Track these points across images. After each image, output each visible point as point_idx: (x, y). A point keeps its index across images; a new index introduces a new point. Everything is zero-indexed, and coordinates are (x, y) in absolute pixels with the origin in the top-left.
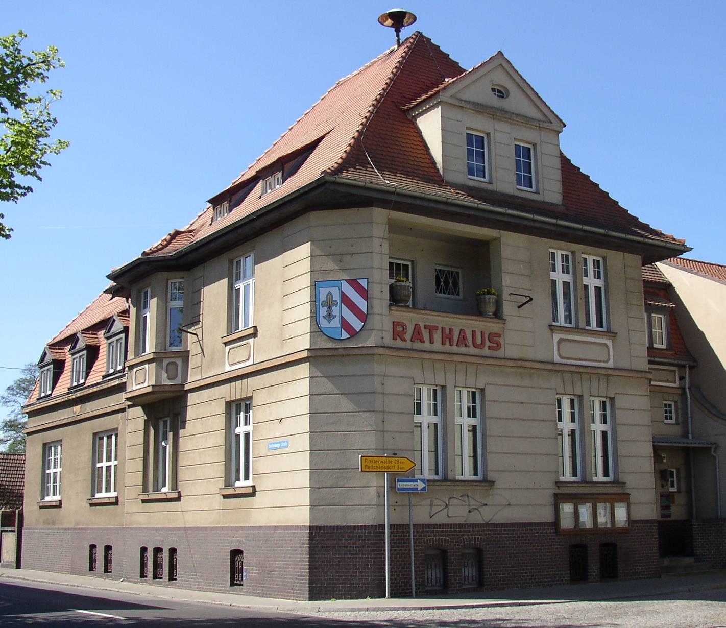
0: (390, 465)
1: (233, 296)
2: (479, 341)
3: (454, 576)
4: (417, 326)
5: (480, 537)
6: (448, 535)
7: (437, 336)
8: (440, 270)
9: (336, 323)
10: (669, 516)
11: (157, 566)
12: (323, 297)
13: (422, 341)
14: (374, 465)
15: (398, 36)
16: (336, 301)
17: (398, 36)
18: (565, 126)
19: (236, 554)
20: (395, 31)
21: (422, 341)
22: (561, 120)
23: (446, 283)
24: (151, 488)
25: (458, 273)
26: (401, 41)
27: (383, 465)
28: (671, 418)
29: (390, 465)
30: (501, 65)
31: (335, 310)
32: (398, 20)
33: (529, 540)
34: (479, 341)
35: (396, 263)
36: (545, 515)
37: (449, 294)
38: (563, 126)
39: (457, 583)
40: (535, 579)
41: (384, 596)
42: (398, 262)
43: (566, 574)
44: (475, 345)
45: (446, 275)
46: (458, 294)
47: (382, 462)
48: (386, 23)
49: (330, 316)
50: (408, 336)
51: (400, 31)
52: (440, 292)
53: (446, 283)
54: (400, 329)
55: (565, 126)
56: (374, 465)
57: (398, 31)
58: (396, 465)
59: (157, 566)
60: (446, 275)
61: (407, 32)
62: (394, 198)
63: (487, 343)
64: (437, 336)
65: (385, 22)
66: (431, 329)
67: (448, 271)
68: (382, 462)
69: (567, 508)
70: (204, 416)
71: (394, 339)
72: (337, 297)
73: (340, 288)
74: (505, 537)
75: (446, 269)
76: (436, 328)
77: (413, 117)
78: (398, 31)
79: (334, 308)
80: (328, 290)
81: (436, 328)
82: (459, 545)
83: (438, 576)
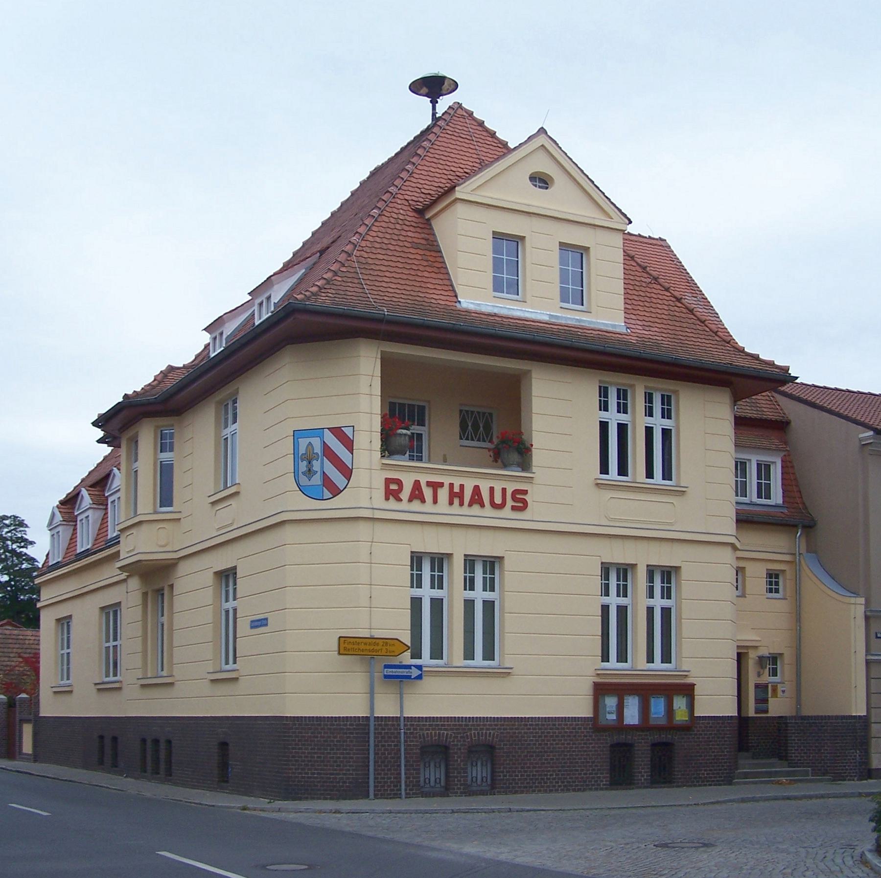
0: (376, 647)
1: (224, 449)
2: (498, 500)
3: (457, 777)
4: (417, 484)
5: (492, 732)
6: (452, 729)
7: (443, 494)
8: (467, 411)
9: (317, 480)
10: (767, 711)
11: (156, 761)
12: (302, 450)
13: (423, 501)
14: (356, 647)
15: (434, 108)
16: (317, 454)
17: (434, 108)
18: (630, 222)
19: (224, 745)
20: (431, 102)
21: (423, 501)
22: (625, 216)
23: (476, 427)
24: (111, 674)
25: (491, 414)
26: (437, 115)
27: (368, 647)
28: (777, 591)
29: (376, 647)
30: (542, 146)
31: (316, 465)
32: (432, 86)
33: (557, 736)
34: (498, 500)
35: (399, 404)
36: (582, 709)
37: (479, 440)
38: (627, 222)
39: (461, 785)
40: (563, 782)
41: (367, 796)
42: (401, 401)
43: (604, 777)
44: (494, 505)
45: (475, 417)
46: (491, 441)
47: (370, 644)
48: (422, 92)
49: (310, 472)
50: (405, 494)
51: (437, 102)
52: (467, 439)
53: (476, 427)
54: (394, 487)
55: (630, 222)
56: (356, 647)
57: (434, 103)
58: (384, 648)
59: (156, 761)
60: (475, 417)
61: (444, 103)
62: (383, 327)
63: (510, 503)
64: (443, 494)
65: (419, 90)
66: (435, 486)
67: (478, 413)
68: (365, 644)
69: (611, 702)
70: (194, 586)
71: (387, 499)
72: (318, 449)
73: (322, 437)
74: (525, 733)
75: (476, 409)
76: (441, 485)
77: (428, 220)
78: (434, 103)
79: (314, 462)
80: (308, 440)
81: (441, 485)
82: (464, 741)
83: (484, 775)
